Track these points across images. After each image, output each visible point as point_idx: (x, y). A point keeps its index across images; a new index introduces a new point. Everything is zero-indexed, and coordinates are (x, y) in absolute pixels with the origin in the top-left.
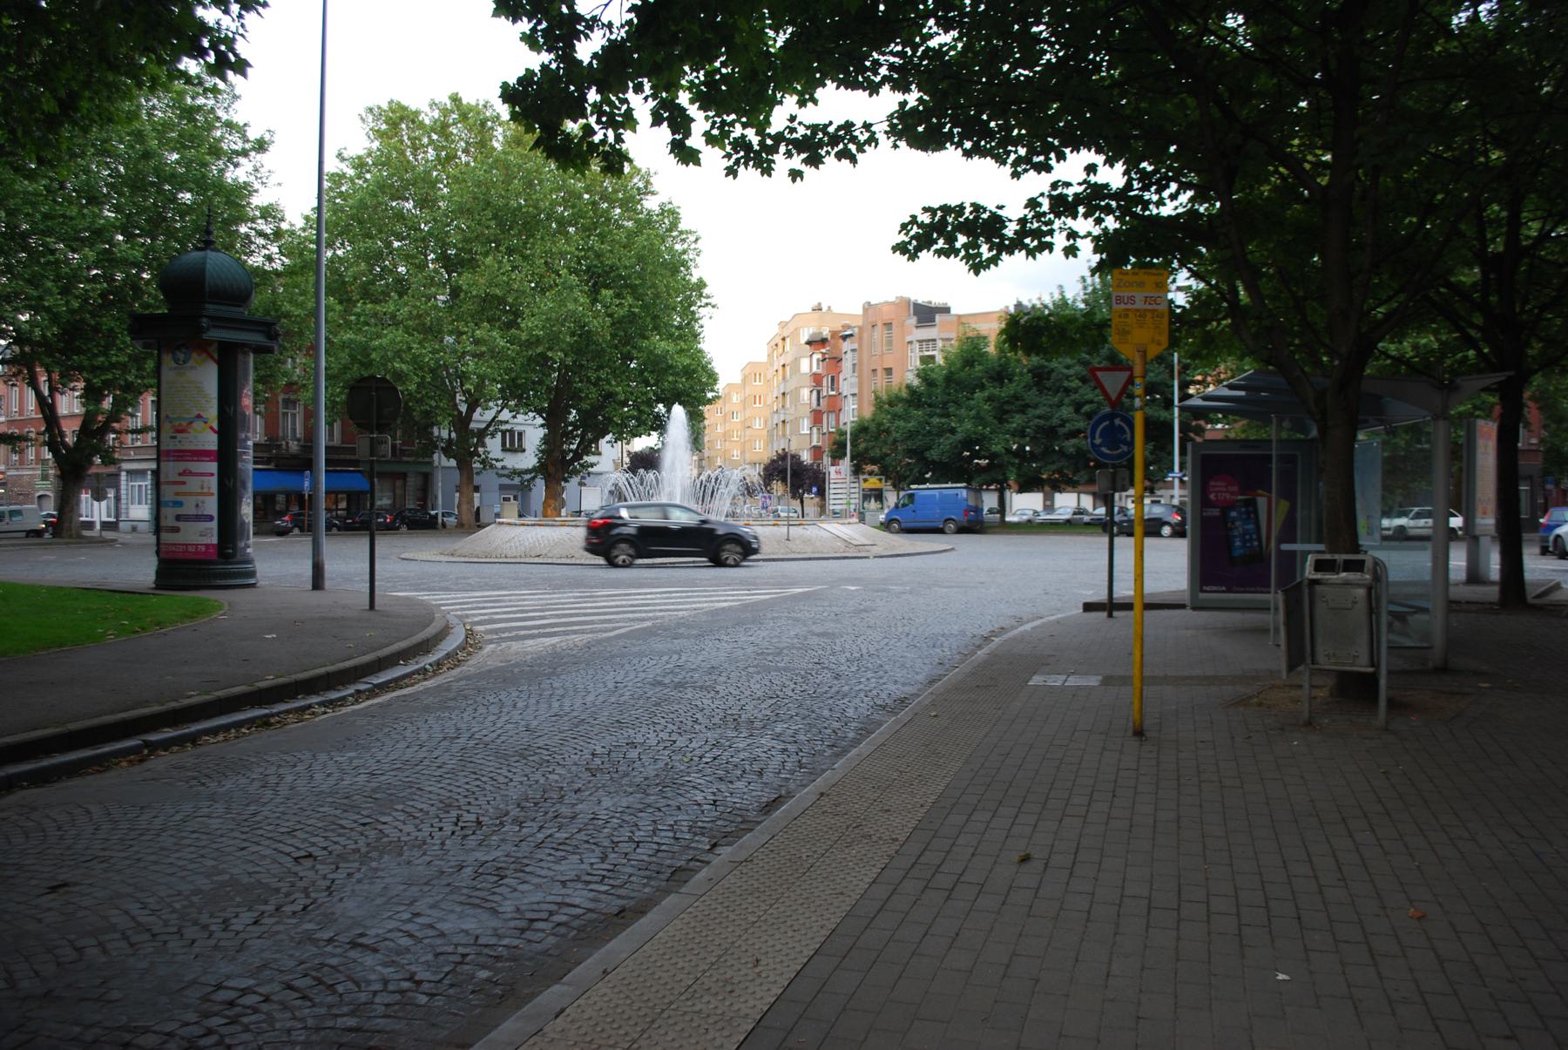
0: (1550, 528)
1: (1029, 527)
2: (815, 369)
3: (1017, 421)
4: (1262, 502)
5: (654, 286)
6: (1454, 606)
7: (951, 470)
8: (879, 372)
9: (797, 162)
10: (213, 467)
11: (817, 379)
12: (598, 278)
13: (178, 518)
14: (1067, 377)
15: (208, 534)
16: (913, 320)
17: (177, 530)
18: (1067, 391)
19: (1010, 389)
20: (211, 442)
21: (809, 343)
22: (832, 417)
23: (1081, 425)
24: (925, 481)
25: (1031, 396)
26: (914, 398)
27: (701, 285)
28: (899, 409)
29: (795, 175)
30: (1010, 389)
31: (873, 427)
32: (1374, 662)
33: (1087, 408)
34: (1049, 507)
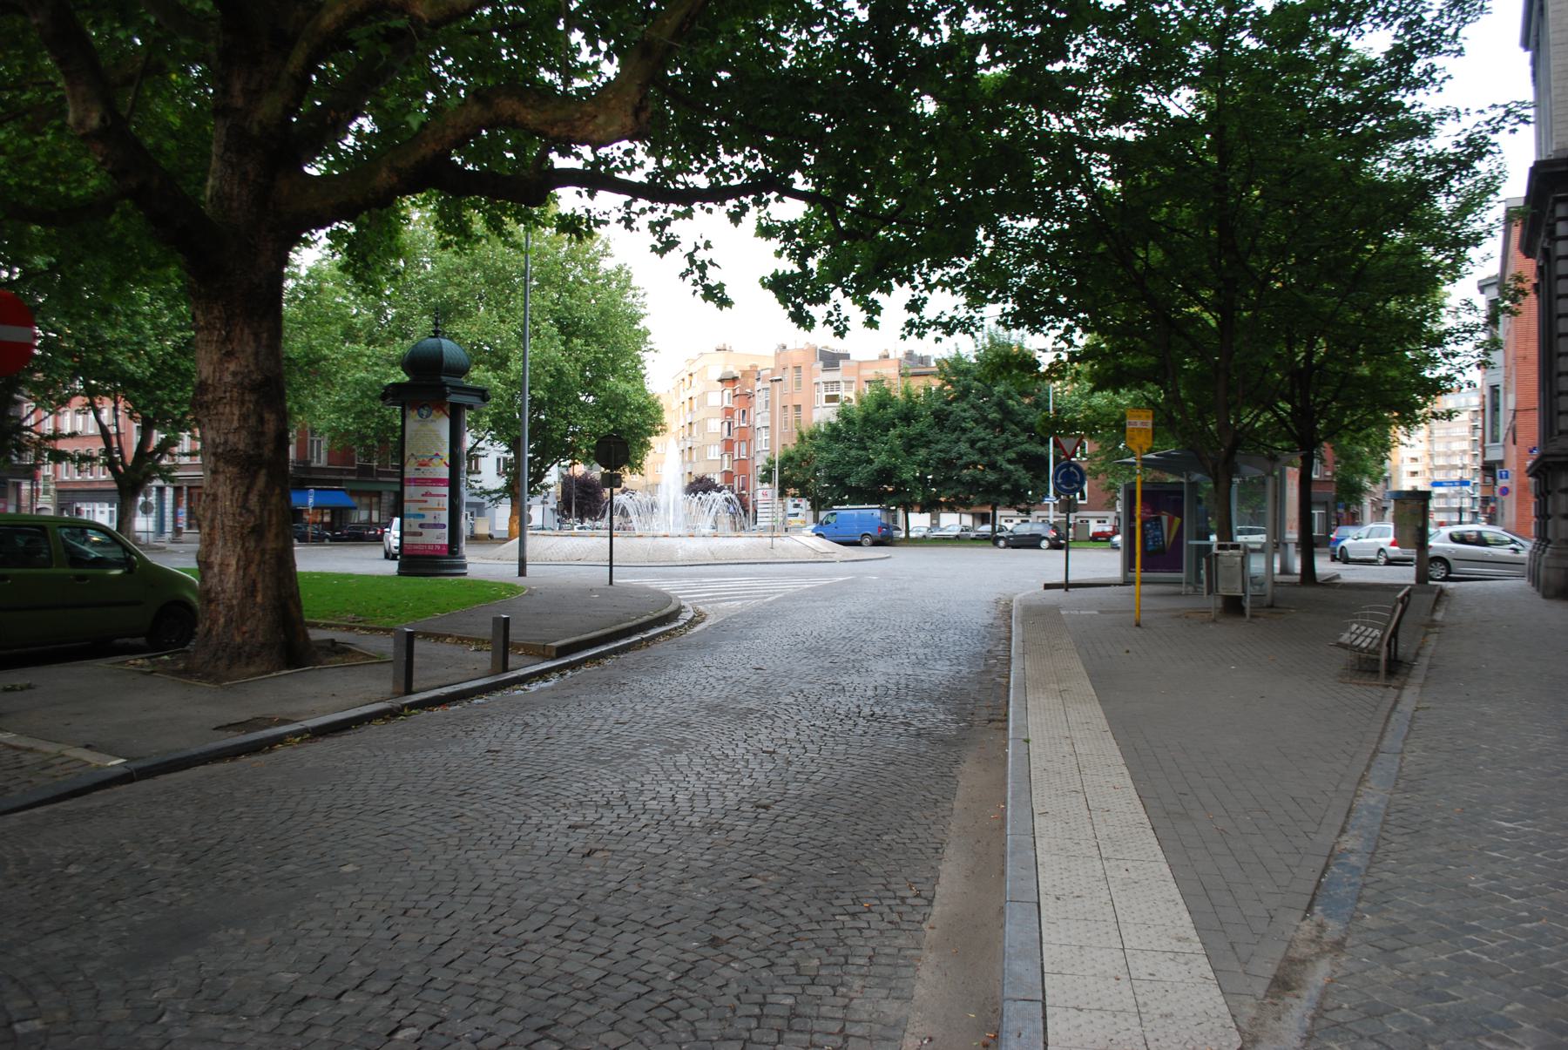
0: (1337, 541)
1: (923, 541)
2: (726, 404)
3: (922, 453)
4: (1165, 518)
5: (615, 335)
6: (1275, 584)
7: (862, 495)
8: (790, 408)
9: (939, 333)
10: (445, 490)
11: (729, 412)
12: (568, 328)
13: (421, 526)
14: (964, 419)
15: (441, 537)
16: (820, 365)
18: (964, 430)
19: (916, 428)
20: (444, 473)
21: (721, 381)
22: (743, 445)
23: (976, 458)
24: (844, 503)
25: (933, 434)
26: (834, 434)
27: (646, 333)
28: (822, 442)
29: (938, 340)
30: (916, 428)
31: (797, 457)
32: (1244, 591)
33: (980, 444)
34: (935, 524)
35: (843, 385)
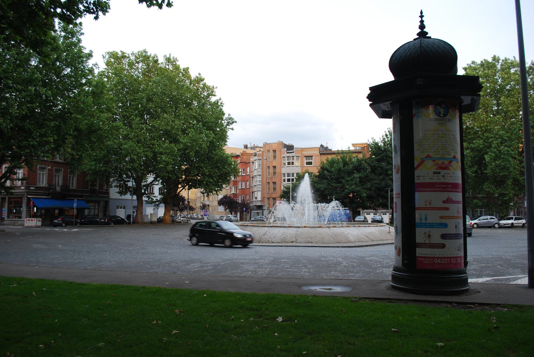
3: (369, 185)
13: (444, 236)
17: (443, 246)
22: (244, 183)
35: (295, 158)
